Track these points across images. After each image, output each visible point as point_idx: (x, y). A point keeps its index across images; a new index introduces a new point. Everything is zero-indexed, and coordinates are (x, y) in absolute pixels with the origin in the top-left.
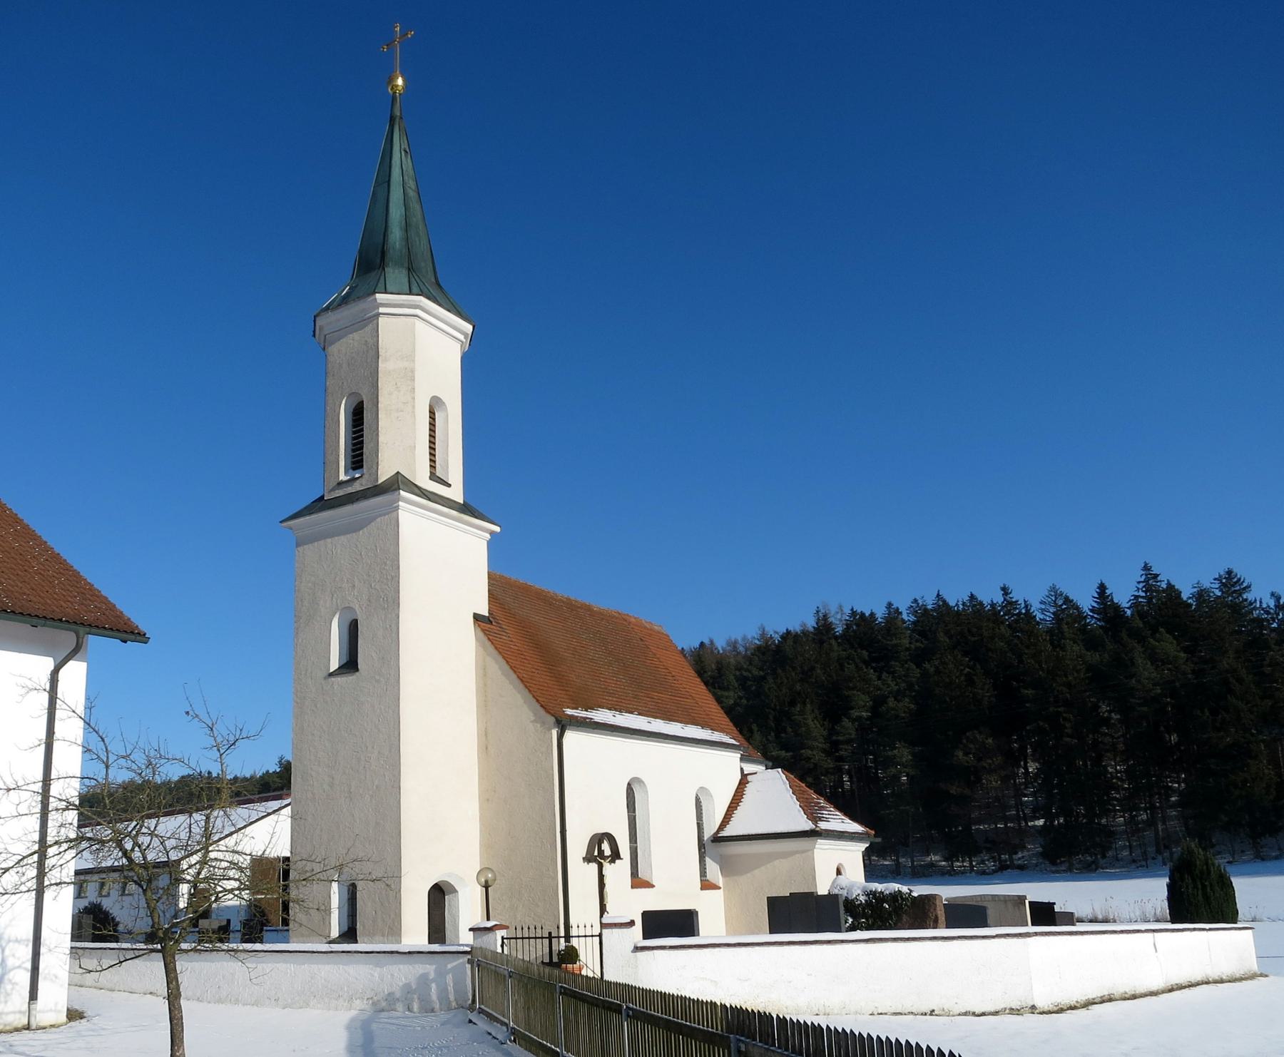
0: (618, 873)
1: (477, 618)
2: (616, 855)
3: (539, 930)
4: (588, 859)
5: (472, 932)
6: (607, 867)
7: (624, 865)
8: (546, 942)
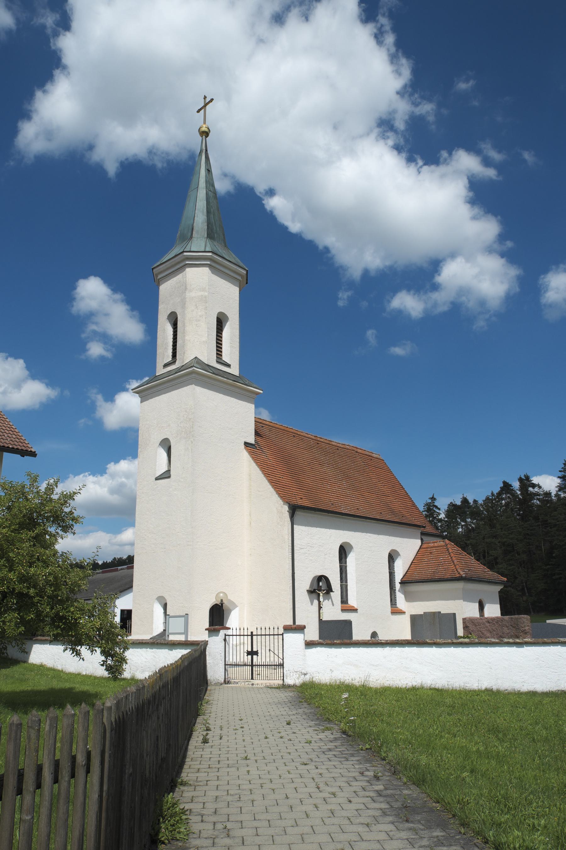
1: (247, 444)
2: (329, 589)
3: (276, 630)
5: (207, 631)
7: (336, 594)
8: (250, 637)
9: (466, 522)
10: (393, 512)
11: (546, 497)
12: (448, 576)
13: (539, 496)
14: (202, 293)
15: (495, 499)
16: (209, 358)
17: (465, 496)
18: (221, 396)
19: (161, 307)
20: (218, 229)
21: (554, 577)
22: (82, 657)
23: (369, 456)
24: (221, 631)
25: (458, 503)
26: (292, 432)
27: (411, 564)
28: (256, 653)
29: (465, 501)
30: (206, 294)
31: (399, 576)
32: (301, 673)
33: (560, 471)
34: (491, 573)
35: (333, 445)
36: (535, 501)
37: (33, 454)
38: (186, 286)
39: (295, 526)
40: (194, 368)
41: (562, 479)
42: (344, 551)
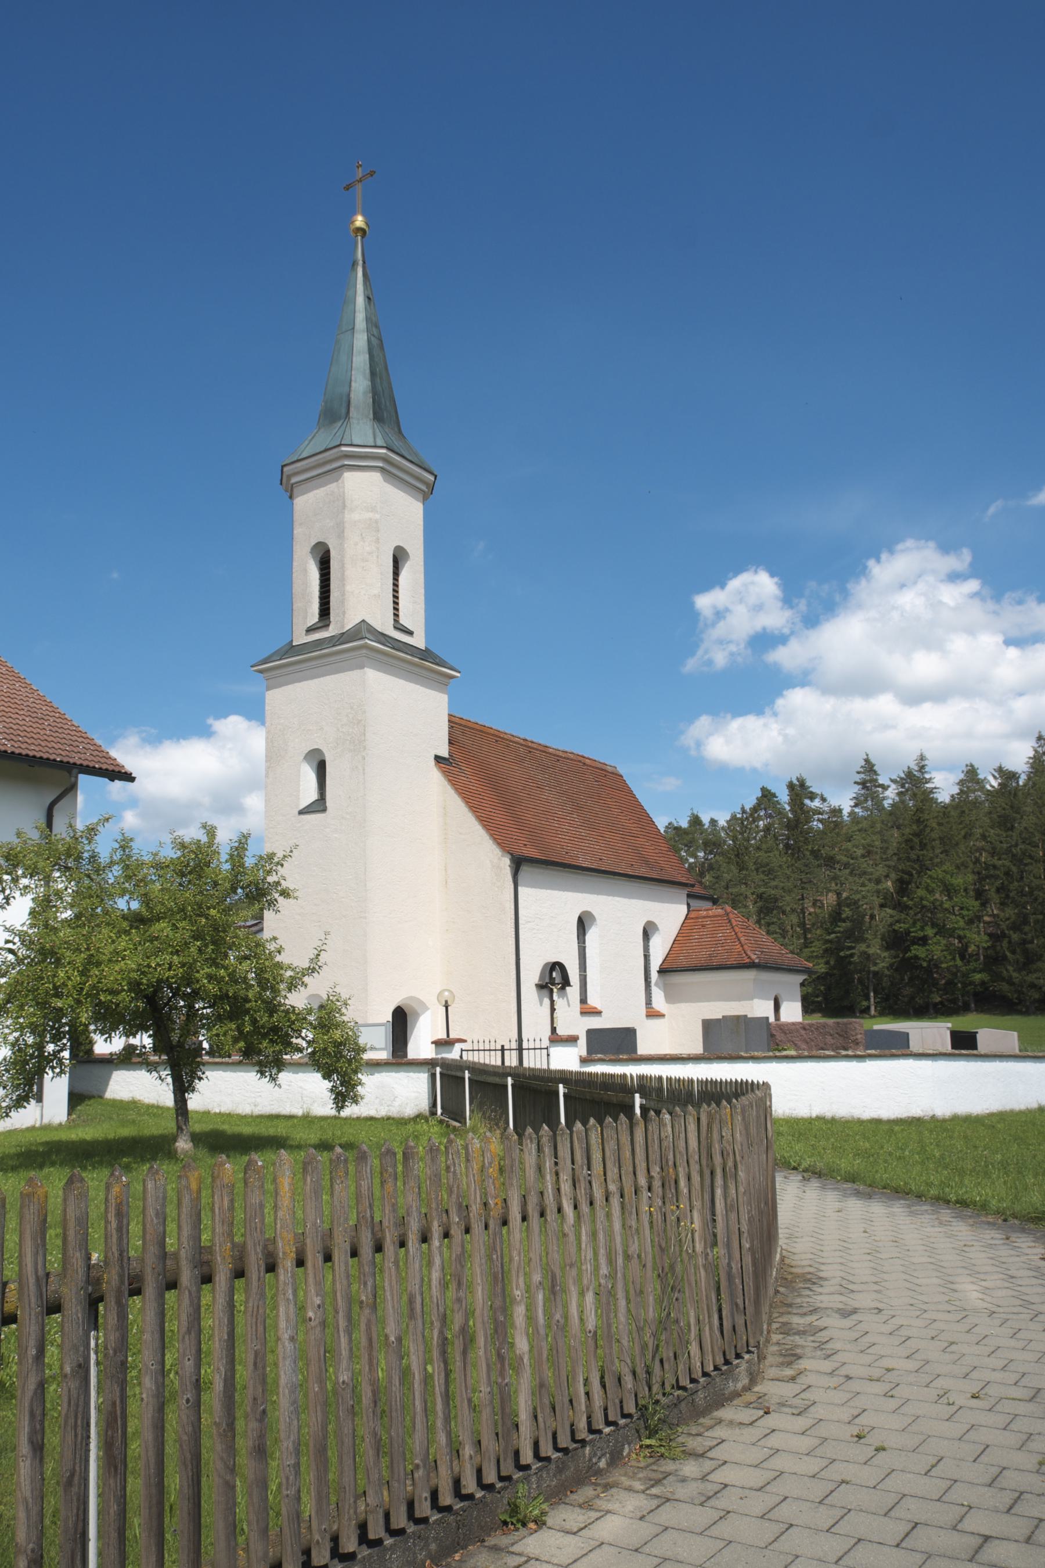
1: (438, 759)
2: (566, 982)
3: (493, 1043)
4: (541, 987)
8: (499, 1053)
9: (696, 857)
10: (646, 862)
11: (835, 816)
12: (732, 961)
13: (822, 814)
14: (370, 515)
15: (747, 818)
16: (383, 623)
17: (695, 813)
18: (402, 682)
19: (298, 531)
20: (388, 404)
21: (842, 954)
22: (278, 1083)
23: (602, 770)
24: (456, 1044)
25: (684, 824)
26: (493, 735)
27: (673, 943)
30: (377, 516)
31: (655, 964)
33: (858, 773)
35: (550, 754)
36: (815, 823)
38: (344, 503)
39: (520, 888)
40: (367, 641)
41: (860, 786)
42: (583, 924)
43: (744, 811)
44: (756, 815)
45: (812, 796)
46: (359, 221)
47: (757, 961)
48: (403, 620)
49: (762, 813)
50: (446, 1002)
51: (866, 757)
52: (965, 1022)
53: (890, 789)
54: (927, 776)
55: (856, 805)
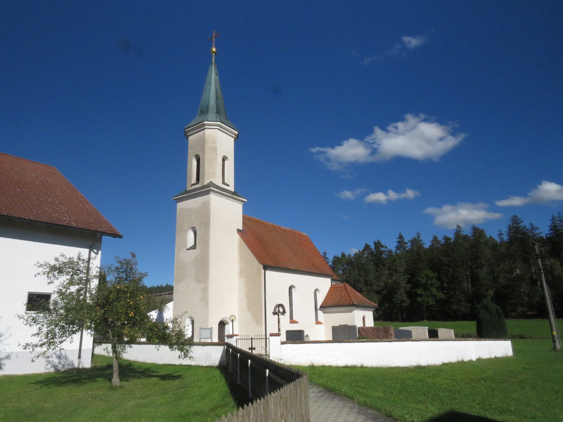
0: (285, 319)
1: (239, 231)
2: (284, 312)
4: (274, 313)
6: (281, 316)
8: (250, 340)
15: (360, 254)
16: (219, 182)
19: (190, 151)
25: (340, 256)
27: (326, 297)
28: (254, 349)
29: (343, 255)
31: (319, 304)
32: (279, 359)
33: (397, 238)
34: (369, 301)
36: (383, 255)
37: (120, 237)
40: (211, 188)
43: (359, 252)
44: (363, 253)
45: (382, 246)
46: (214, 50)
47: (355, 303)
48: (226, 181)
49: (365, 252)
50: (233, 320)
51: (399, 233)
52: (434, 324)
53: (408, 244)
54: (421, 239)
55: (397, 250)
